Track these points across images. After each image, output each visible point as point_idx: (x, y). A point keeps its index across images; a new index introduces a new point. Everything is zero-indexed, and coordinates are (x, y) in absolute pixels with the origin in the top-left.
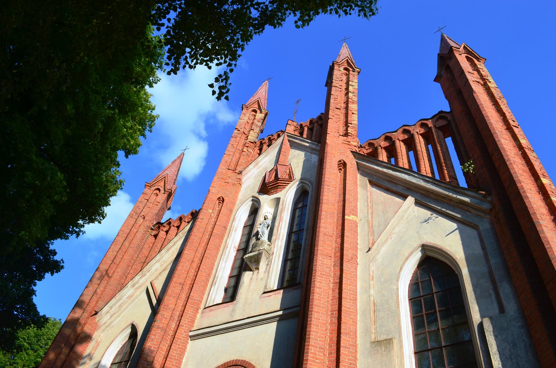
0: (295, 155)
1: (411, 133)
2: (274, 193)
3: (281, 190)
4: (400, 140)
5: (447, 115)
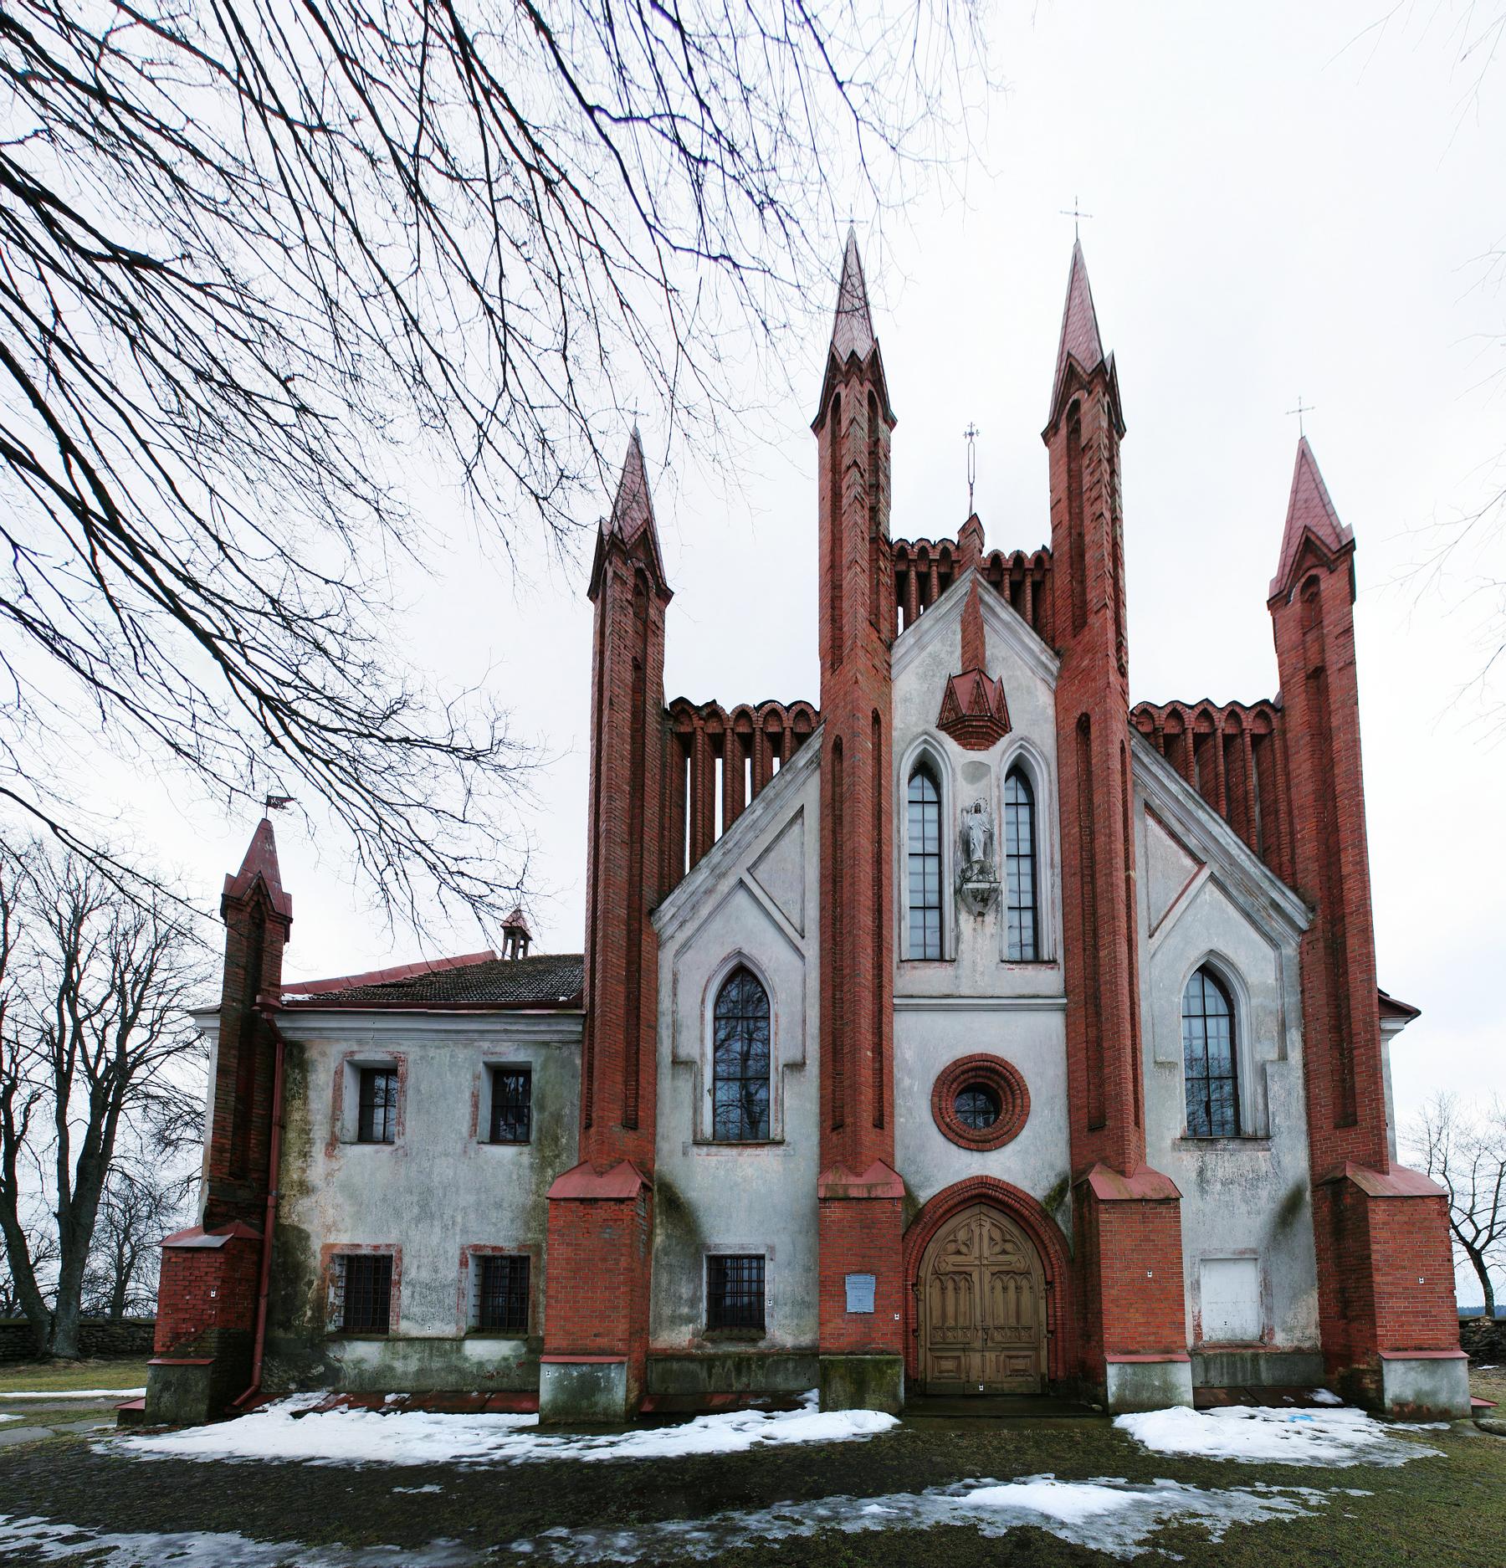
5: (812, 715)
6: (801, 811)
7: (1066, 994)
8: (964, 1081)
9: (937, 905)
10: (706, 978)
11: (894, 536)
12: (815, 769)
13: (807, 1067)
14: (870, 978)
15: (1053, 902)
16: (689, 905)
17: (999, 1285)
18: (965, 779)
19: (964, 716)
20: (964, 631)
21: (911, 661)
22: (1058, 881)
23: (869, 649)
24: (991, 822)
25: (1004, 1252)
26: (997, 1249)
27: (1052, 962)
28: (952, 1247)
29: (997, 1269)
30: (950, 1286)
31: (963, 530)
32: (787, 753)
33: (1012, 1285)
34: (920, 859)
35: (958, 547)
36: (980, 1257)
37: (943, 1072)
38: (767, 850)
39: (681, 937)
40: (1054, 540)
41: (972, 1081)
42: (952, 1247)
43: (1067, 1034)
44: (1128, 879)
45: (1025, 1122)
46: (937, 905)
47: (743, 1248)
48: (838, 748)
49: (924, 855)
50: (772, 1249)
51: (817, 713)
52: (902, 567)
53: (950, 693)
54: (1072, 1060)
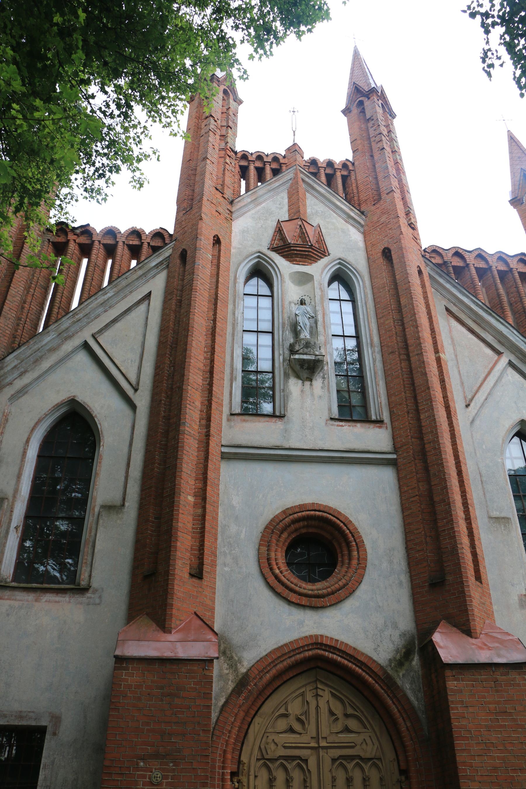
0: (317, 212)
1: (93, 239)
2: (301, 263)
3: (311, 264)
4: (102, 242)
5: (166, 236)
6: (148, 296)
7: (396, 450)
8: (296, 530)
9: (271, 370)
10: (36, 420)
11: (239, 148)
12: (164, 269)
13: (126, 509)
14: (196, 427)
15: (375, 373)
16: (32, 359)
17: (341, 776)
18: (293, 282)
19: (290, 244)
20: (289, 198)
21: (249, 211)
22: (378, 357)
23: (214, 201)
24: (315, 312)
25: (347, 730)
26: (339, 727)
27: (379, 422)
28: (282, 724)
29: (337, 753)
30: (280, 776)
31: (288, 150)
32: (143, 258)
33: (357, 776)
34: (255, 334)
35: (284, 157)
36: (317, 738)
37: (272, 520)
38: (115, 321)
39: (19, 384)
40: (353, 157)
41: (304, 531)
42: (282, 724)
43: (400, 488)
44: (439, 360)
45: (362, 576)
46: (271, 370)
47: (21, 717)
48: (183, 256)
49: (257, 332)
50: (57, 719)
51: (171, 236)
52: (244, 163)
53: (279, 230)
54: (406, 513)
